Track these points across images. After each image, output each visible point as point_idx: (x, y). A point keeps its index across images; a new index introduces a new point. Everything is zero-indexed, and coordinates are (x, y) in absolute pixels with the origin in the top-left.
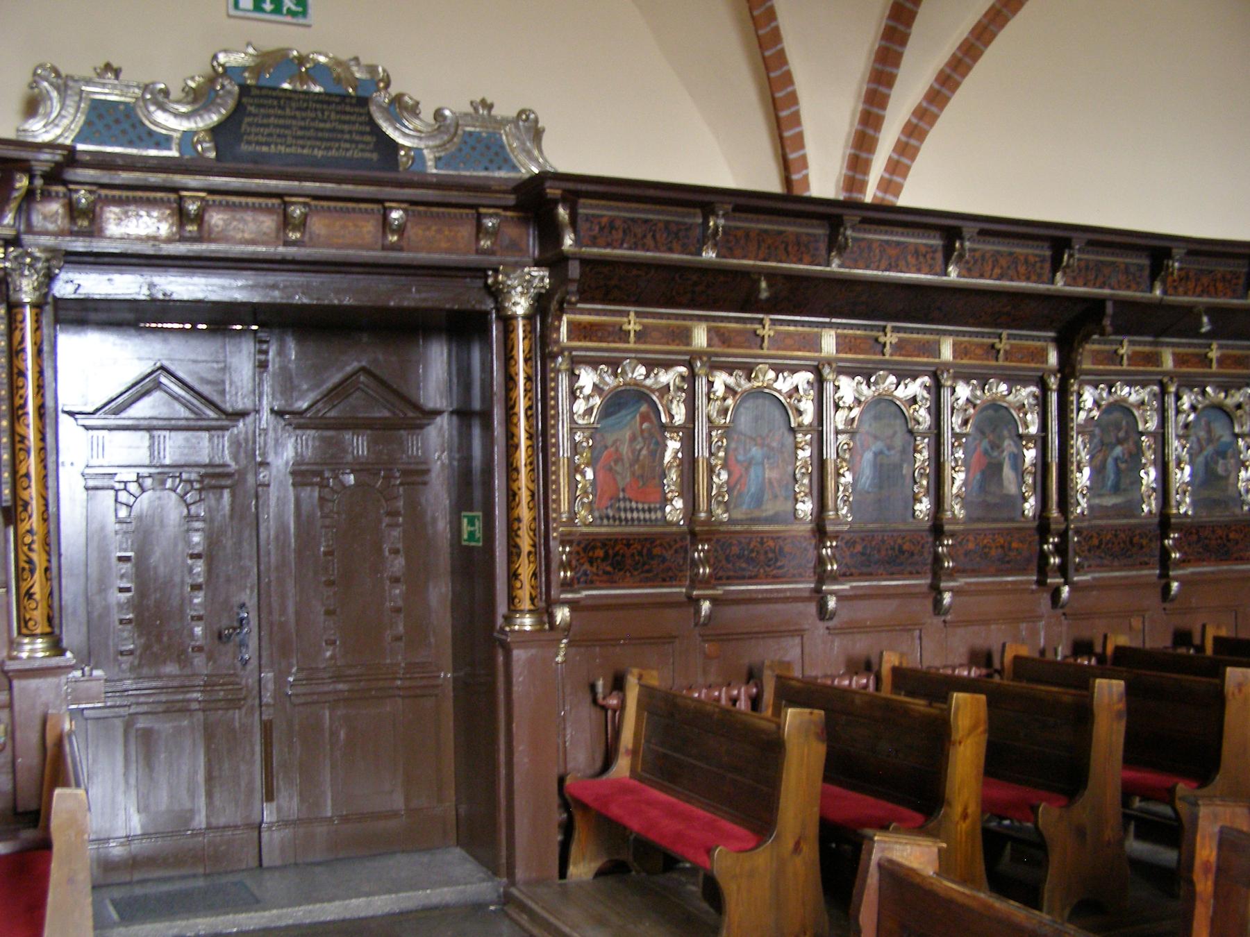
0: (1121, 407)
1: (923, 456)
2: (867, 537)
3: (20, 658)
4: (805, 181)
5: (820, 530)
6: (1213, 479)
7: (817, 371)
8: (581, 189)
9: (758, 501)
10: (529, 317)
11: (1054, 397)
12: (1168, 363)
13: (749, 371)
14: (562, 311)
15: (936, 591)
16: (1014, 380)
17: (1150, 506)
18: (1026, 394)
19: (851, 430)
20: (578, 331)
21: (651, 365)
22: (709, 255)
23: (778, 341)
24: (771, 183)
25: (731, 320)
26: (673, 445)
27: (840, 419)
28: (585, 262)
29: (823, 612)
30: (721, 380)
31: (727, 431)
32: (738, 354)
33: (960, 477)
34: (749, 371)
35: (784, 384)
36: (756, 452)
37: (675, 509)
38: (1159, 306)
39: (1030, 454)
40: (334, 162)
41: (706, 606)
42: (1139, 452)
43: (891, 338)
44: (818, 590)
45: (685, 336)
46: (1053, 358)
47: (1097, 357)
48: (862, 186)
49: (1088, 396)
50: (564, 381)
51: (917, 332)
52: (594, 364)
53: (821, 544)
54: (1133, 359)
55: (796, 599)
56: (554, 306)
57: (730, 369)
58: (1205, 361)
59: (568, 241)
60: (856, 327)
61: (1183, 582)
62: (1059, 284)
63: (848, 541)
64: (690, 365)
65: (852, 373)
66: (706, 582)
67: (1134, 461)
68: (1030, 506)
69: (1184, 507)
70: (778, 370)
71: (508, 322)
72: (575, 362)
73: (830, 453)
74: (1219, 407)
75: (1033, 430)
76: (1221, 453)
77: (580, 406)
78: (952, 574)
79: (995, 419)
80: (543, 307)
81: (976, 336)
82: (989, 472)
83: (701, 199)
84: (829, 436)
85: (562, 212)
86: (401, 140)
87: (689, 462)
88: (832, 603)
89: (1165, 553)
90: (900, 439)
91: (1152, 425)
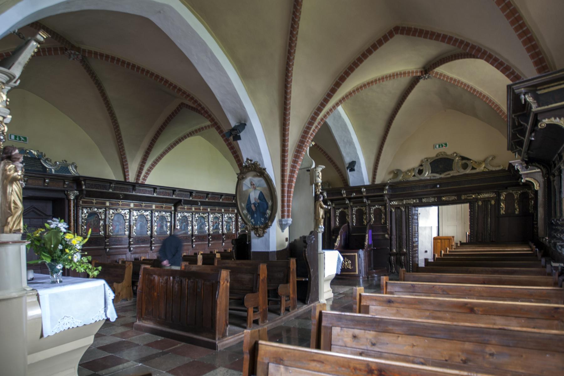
0: (185, 216)
1: (149, 224)
2: (138, 238)
3: (524, 88)
4: (129, 178)
5: (130, 237)
6: (201, 228)
7: (130, 210)
8: (86, 179)
9: (118, 231)
10: (74, 200)
11: (173, 215)
12: (193, 209)
13: (116, 210)
14: (81, 198)
15: (151, 247)
16: (166, 212)
17: (190, 233)
18: (168, 214)
19: (136, 220)
20: (83, 202)
21: (98, 208)
22: (111, 191)
23: (122, 205)
24: (122, 179)
25: (114, 201)
26: (102, 222)
27: (134, 218)
28: (87, 191)
29: (130, 250)
30: (111, 211)
31: (112, 220)
32: (114, 207)
33: (156, 228)
34: (116, 210)
35: (123, 212)
36: (117, 223)
37: (102, 233)
38: (191, 201)
39: (169, 224)
40: (35, 171)
41: (108, 250)
42: (188, 224)
43: (144, 205)
44: (129, 247)
45: (105, 203)
46: (173, 208)
47: (181, 208)
48: (139, 180)
49: (179, 215)
50: (81, 211)
51: (148, 204)
52: (86, 208)
53: (130, 239)
54: (187, 209)
55: (125, 248)
56: (79, 198)
57: (113, 209)
58: (200, 209)
59: (84, 187)
60: (137, 203)
61: (196, 245)
62: (174, 197)
63: (135, 238)
64: (105, 208)
65: (136, 210)
66: (108, 245)
67: (187, 225)
68: (168, 233)
69: (196, 233)
70: (122, 209)
71: (69, 200)
72: (83, 208)
73: (132, 224)
74: (202, 217)
75: (169, 220)
76: (203, 224)
77: (83, 215)
78: (154, 244)
79: (162, 218)
80: (77, 198)
81: (159, 204)
82: (162, 227)
83: (110, 182)
84: (132, 221)
85: (83, 182)
86: (47, 166)
87: (105, 226)
88: (132, 249)
89: (192, 240)
90: (145, 221)
91: (190, 219)
